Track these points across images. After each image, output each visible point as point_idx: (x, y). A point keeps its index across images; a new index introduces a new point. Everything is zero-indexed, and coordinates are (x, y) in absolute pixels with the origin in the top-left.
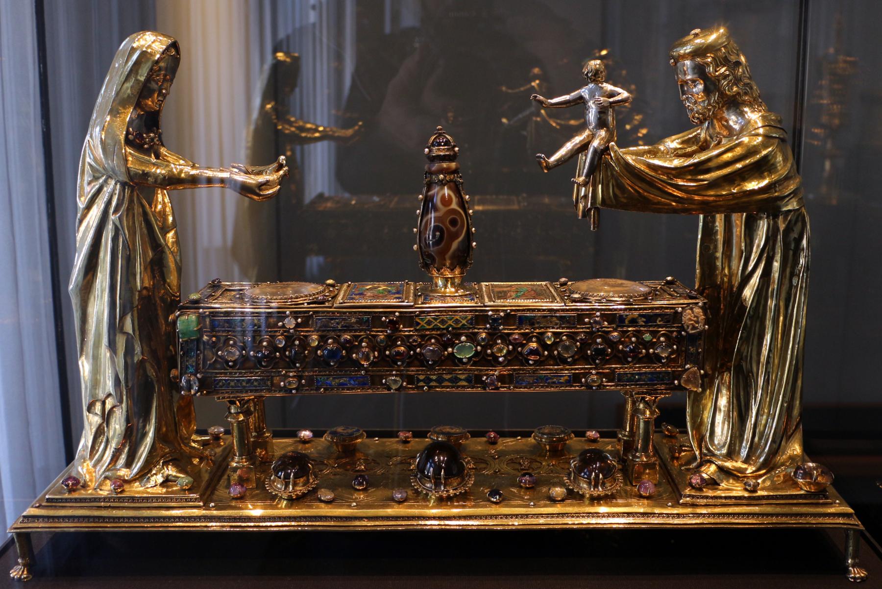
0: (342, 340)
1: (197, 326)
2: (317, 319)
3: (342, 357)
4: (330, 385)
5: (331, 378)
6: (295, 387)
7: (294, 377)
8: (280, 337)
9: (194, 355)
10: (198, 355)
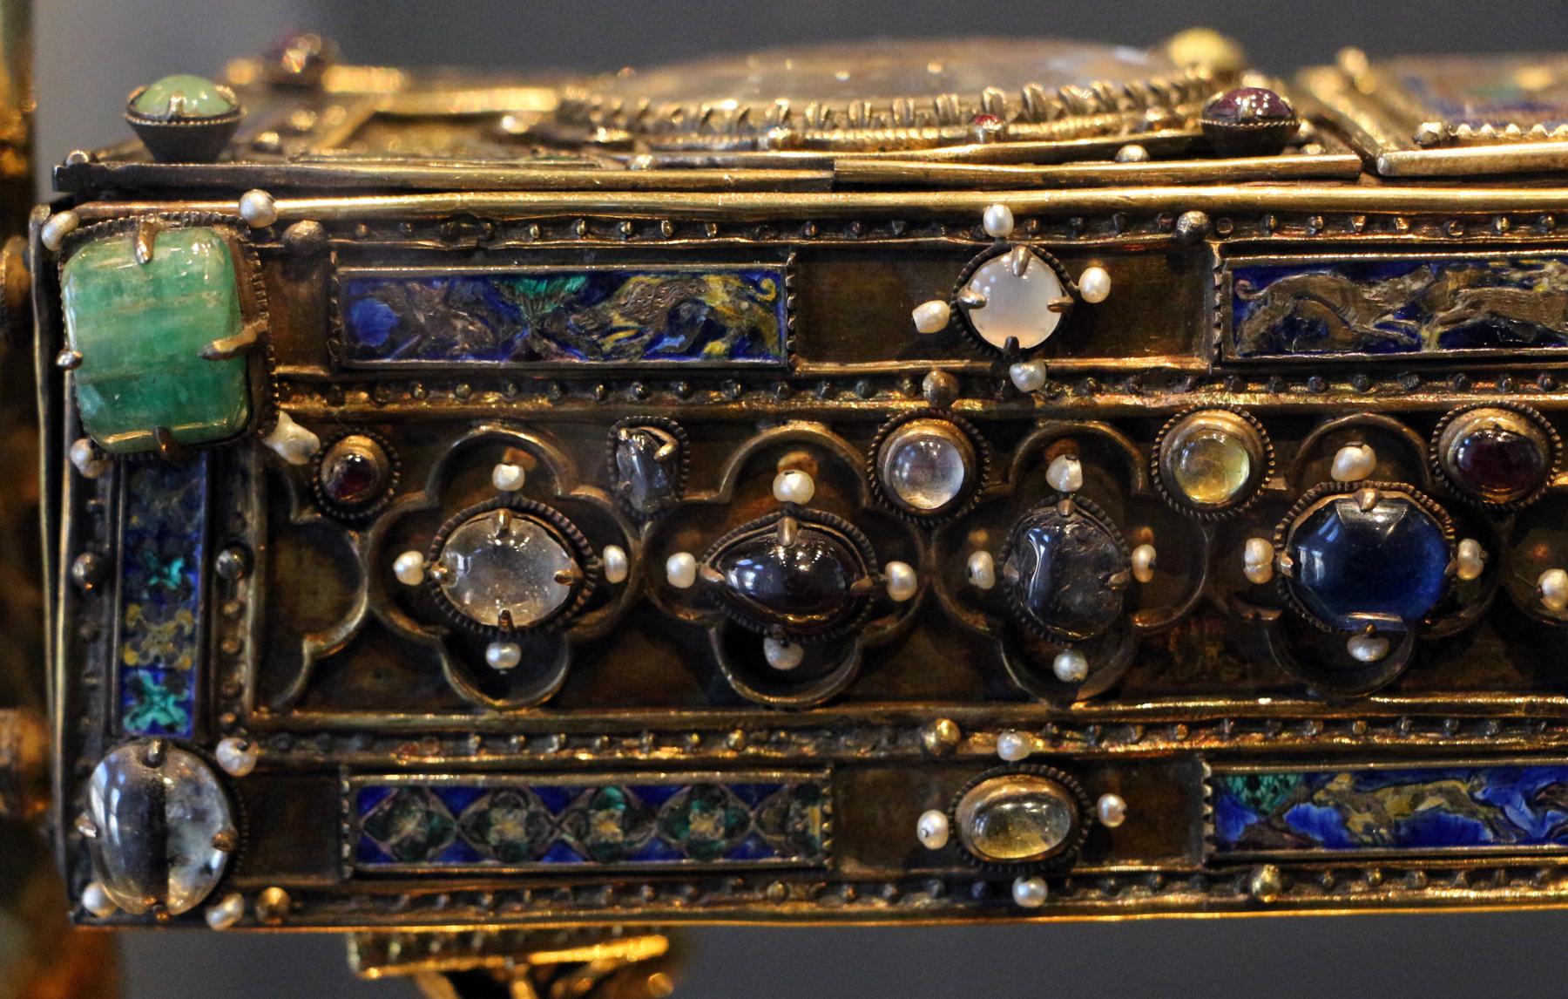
0: (1453, 443)
1: (231, 329)
2: (1239, 272)
3: (1451, 595)
4: (1334, 841)
5: (1343, 783)
6: (1038, 849)
7: (1032, 765)
8: (915, 430)
9: (186, 588)
10: (220, 587)
